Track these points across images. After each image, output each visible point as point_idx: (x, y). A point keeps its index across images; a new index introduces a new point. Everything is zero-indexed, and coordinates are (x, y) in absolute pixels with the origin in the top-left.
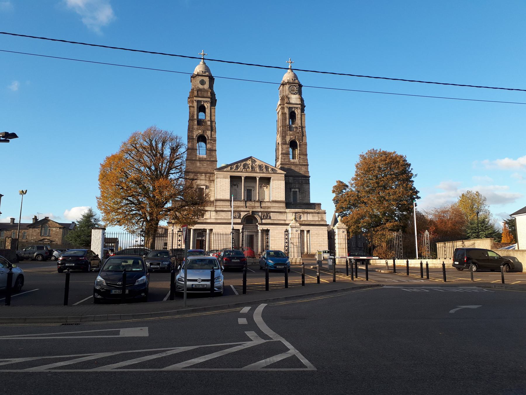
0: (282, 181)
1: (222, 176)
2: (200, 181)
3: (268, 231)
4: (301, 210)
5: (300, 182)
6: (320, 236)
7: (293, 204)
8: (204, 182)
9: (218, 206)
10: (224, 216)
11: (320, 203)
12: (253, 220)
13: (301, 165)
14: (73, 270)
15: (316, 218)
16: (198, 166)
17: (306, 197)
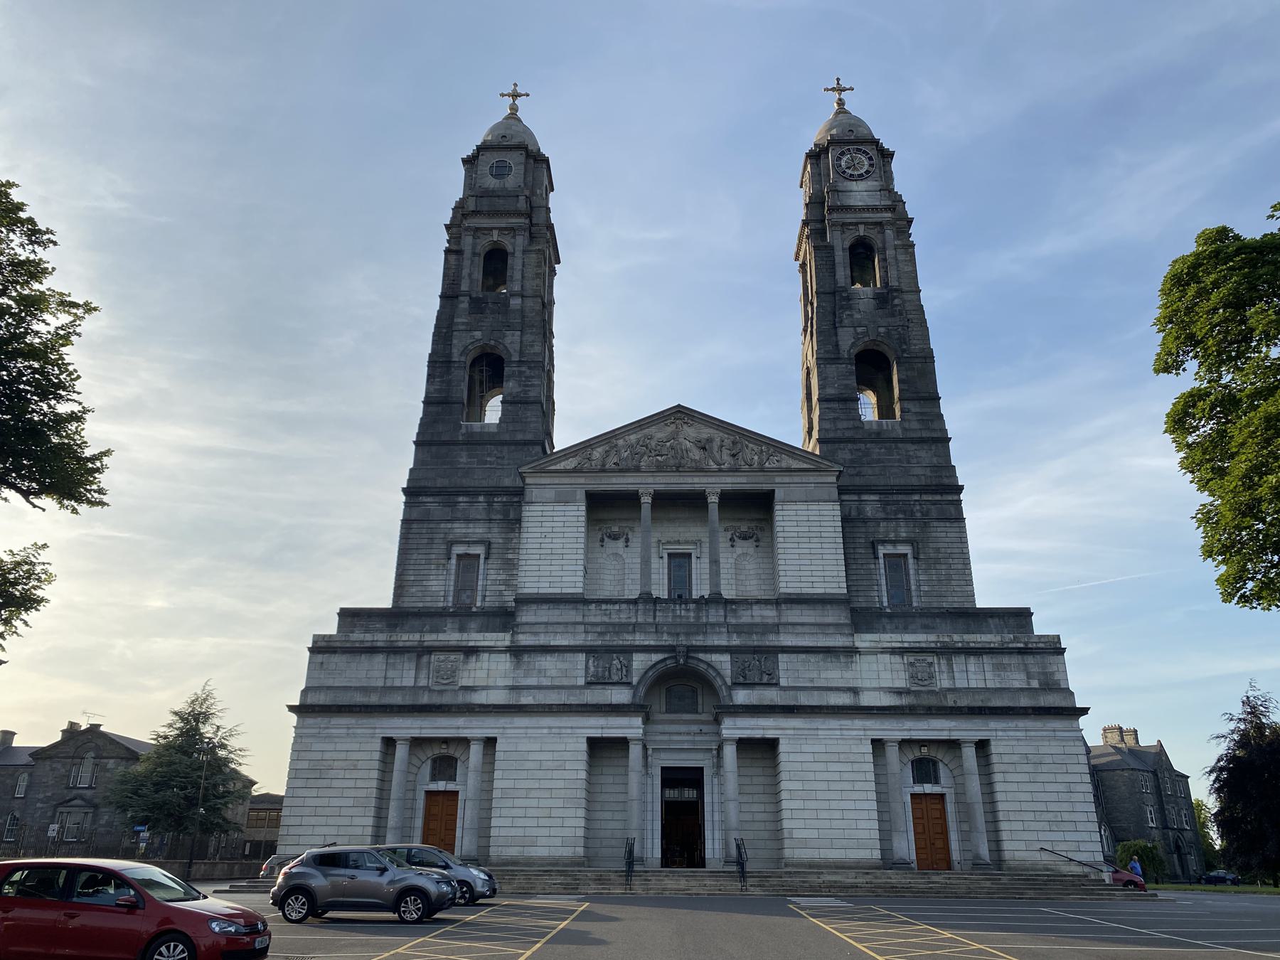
0: (829, 506)
1: (550, 494)
3: (770, 746)
4: (932, 637)
6: (1045, 768)
7: (890, 617)
8: (481, 531)
9: (527, 628)
10: (554, 673)
11: (1028, 609)
12: (699, 692)
13: (913, 441)
14: (1223, 819)
15: (1017, 680)
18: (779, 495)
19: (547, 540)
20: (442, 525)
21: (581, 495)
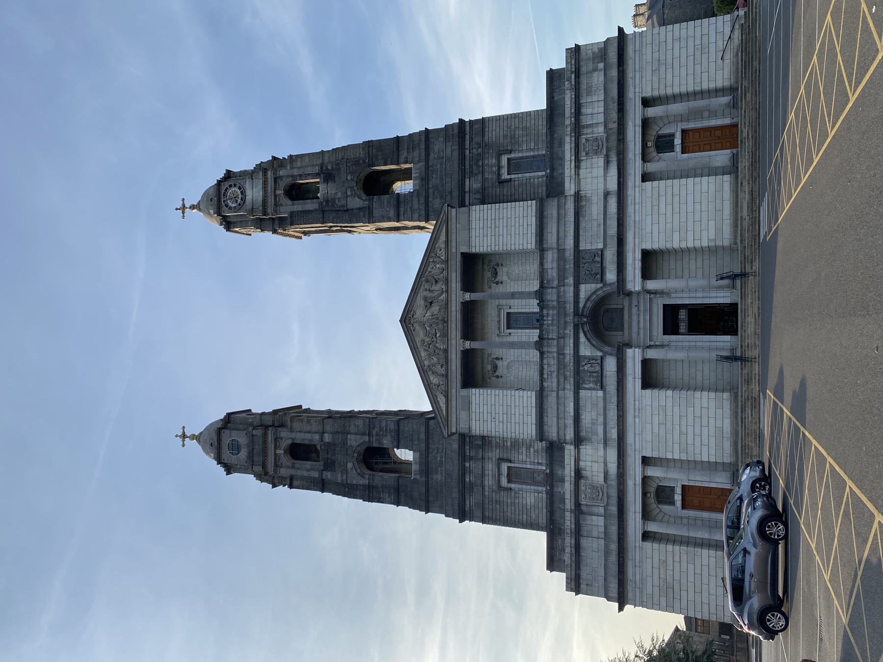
0: (473, 214)
1: (463, 415)
2: (487, 478)
3: (647, 256)
5: (480, 150)
6: (662, 57)
7: (553, 169)
8: (490, 465)
9: (561, 432)
10: (594, 413)
11: (547, 72)
12: (608, 307)
13: (427, 155)
15: (598, 79)
16: (444, 478)
17: (528, 125)
18: (464, 249)
19: (497, 418)
20: (487, 493)
21: (464, 392)
